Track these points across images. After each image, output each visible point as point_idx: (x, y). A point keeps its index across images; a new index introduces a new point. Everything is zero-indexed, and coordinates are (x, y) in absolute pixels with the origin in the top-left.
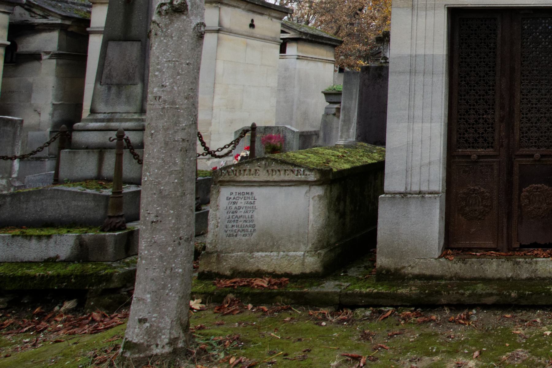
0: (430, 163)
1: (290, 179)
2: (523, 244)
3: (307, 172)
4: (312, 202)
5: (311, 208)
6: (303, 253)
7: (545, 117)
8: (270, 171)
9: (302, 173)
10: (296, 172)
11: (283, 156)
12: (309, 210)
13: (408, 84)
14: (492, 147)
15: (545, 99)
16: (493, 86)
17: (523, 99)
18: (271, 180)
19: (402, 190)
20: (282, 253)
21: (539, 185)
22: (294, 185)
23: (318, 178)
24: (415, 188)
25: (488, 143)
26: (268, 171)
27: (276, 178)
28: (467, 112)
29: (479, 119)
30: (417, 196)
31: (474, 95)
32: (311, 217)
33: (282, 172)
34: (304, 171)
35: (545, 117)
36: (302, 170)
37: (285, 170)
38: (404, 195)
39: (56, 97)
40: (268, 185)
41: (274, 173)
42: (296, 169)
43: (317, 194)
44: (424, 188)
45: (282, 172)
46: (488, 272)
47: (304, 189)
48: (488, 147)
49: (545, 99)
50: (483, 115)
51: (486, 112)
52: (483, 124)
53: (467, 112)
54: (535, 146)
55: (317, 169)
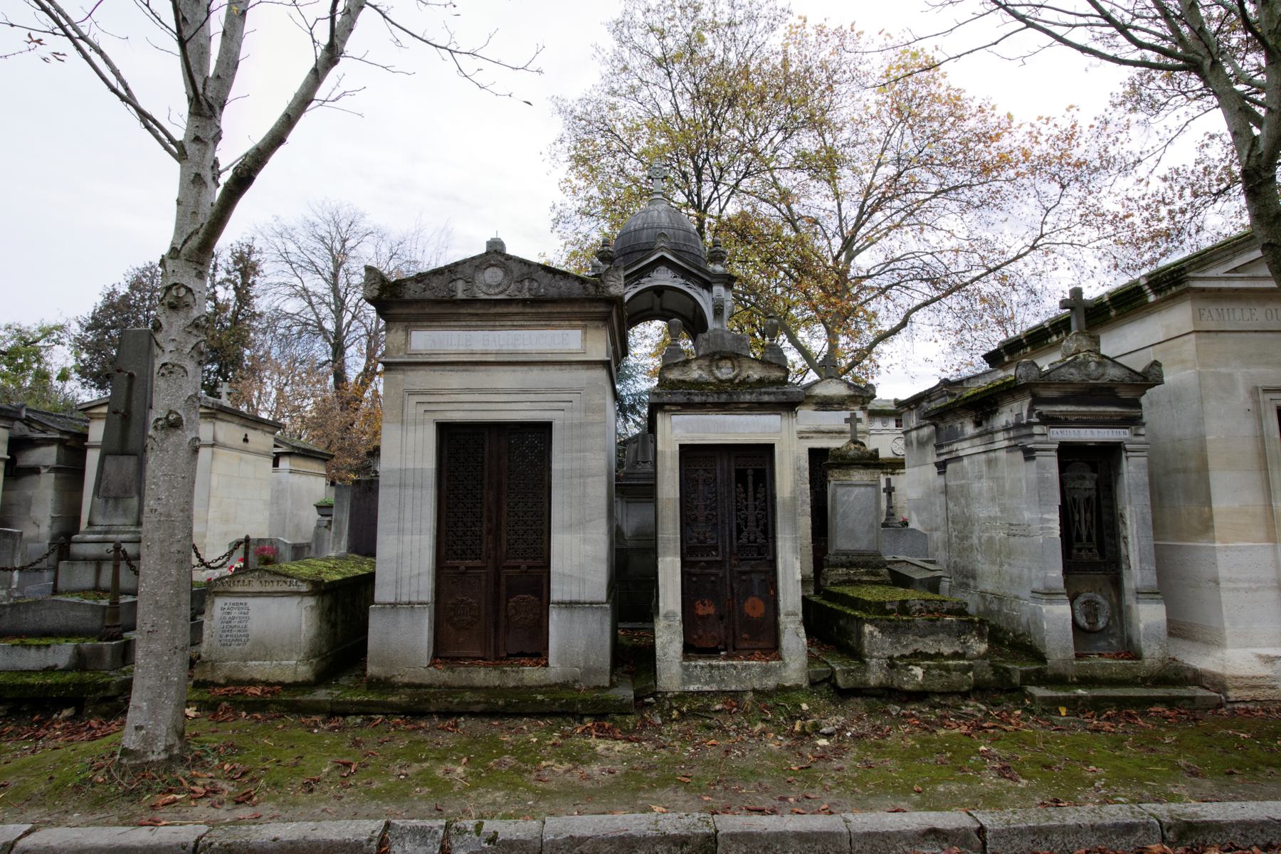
19: (393, 600)
24: (405, 599)
27: (269, 588)
32: (304, 627)
44: (414, 599)
47: (296, 600)
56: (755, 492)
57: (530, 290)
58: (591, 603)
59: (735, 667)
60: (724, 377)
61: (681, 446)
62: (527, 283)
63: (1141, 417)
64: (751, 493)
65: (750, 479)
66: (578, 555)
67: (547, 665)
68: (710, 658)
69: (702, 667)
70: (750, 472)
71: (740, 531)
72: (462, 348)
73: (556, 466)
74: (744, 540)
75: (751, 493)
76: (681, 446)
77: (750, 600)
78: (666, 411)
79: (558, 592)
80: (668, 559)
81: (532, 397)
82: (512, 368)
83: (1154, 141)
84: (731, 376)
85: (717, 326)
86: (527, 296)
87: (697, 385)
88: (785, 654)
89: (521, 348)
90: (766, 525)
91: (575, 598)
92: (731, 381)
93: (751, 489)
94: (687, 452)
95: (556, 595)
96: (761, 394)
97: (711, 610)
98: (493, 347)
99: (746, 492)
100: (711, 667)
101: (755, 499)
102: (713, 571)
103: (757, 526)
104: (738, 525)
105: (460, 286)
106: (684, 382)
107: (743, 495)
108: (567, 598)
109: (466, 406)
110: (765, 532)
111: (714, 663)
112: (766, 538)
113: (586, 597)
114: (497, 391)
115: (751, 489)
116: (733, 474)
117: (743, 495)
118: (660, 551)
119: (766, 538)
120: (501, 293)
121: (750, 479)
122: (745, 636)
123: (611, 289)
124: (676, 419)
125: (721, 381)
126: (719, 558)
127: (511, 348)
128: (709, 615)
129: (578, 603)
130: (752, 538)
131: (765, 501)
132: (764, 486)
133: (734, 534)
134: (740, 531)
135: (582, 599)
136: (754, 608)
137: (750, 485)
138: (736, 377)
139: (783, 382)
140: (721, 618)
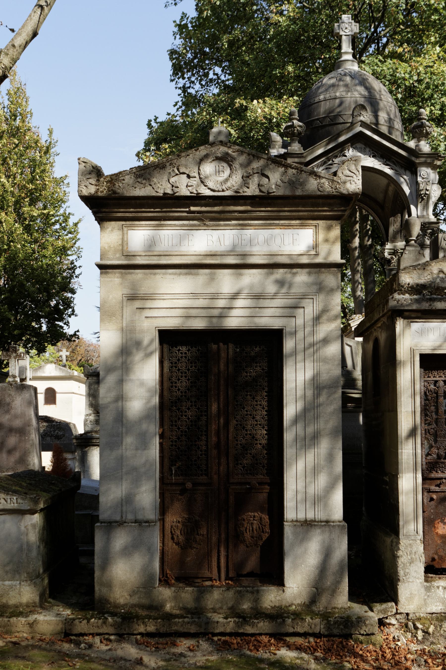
30: (133, 524)
34: (17, 499)
78: (405, 318)
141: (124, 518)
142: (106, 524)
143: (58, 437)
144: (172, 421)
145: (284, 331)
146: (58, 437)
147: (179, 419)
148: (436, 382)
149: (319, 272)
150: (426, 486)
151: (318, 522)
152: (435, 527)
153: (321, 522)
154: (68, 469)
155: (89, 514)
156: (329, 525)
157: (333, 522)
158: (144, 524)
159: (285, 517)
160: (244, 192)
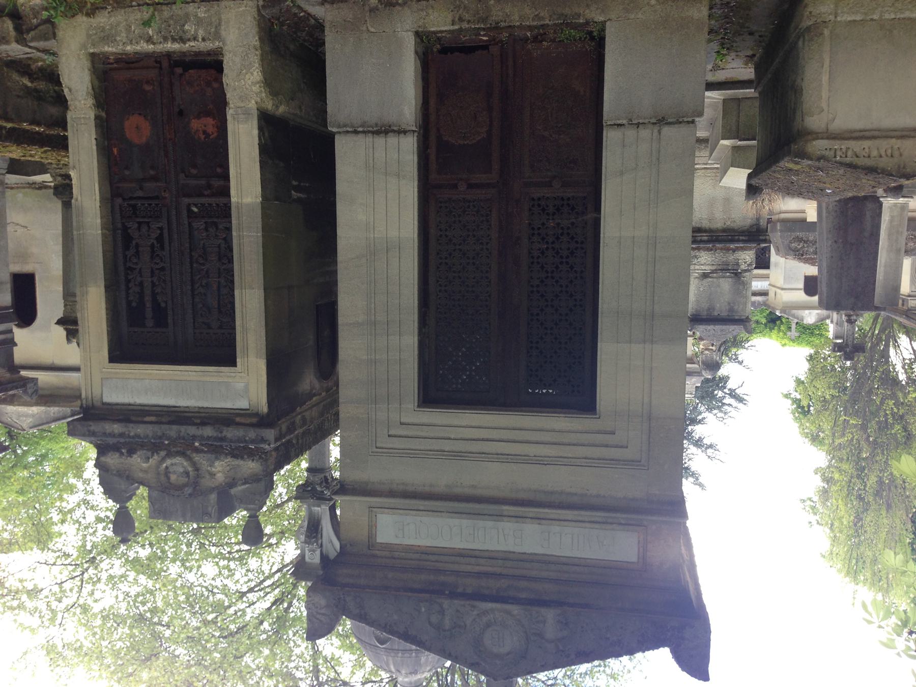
0: (622, 173)
1: (860, 142)
2: (485, 52)
3: (830, 154)
4: (824, 105)
5: (825, 94)
6: (839, 19)
7: (455, 244)
8: (896, 153)
9: (839, 153)
10: (850, 153)
11: (65, 421)
12: (830, 91)
13: (656, 298)
14: (533, 199)
15: (454, 272)
16: (532, 292)
17: (487, 272)
18: (894, 140)
19: (666, 130)
20: (875, 17)
21: (461, 142)
22: (855, 131)
23: (809, 145)
24: (645, 133)
25: (539, 205)
26: (901, 155)
27: (884, 145)
28: (572, 253)
29: (553, 243)
30: (641, 121)
31: (560, 278)
32: (825, 78)
33: (875, 153)
34: (835, 157)
35: (455, 244)
36: (838, 158)
37: (869, 157)
38: (661, 122)
39: (96, 134)
40: (903, 130)
41: (889, 152)
42: (848, 160)
43: (815, 117)
44: (631, 133)
45: (875, 153)
46: (813, 271)
47: (839, 124)
48: (539, 199)
49: (454, 272)
50: (547, 249)
51: (543, 253)
52: (547, 235)
53: (572, 253)
54: (469, 202)
55: (809, 158)
56: (141, 295)
57: (442, 612)
58: (356, 132)
59: (149, 40)
60: (178, 460)
61: (233, 363)
62: (447, 623)
63: (13, 339)
64: (148, 292)
65: (149, 313)
66: (379, 205)
67: (417, 34)
68: (183, 54)
69: (195, 39)
70: (150, 323)
71: (160, 239)
72: (556, 528)
73: (411, 341)
74: (155, 225)
75: (148, 292)
76: (233, 363)
77: (144, 140)
78: (256, 414)
79: (407, 148)
80: (248, 200)
81: (447, 446)
82: (479, 492)
83: (235, 589)
84: (169, 462)
85: (316, 509)
86: (446, 603)
87: (216, 449)
88: (87, 64)
89: (465, 522)
90: (127, 247)
91: (380, 141)
92: (169, 455)
93: (148, 298)
94: (223, 354)
95: (409, 145)
96: (121, 435)
97: (196, 125)
98: (508, 526)
99: (154, 295)
100: (183, 40)
101: (141, 284)
102: (193, 182)
103: (137, 246)
104: (162, 248)
105: (551, 631)
106: (235, 456)
107: (158, 290)
108: (392, 140)
109: (547, 437)
110: (127, 239)
111: (176, 46)
112: (125, 229)
113: (363, 141)
114: (501, 457)
115: (148, 298)
116: (170, 321)
117: (158, 290)
118: (259, 211)
119: (125, 229)
120: (485, 612)
121: (149, 313)
122: (147, 88)
123: (323, 602)
124: (242, 404)
125: (183, 454)
126: (186, 200)
127: (481, 523)
128: (198, 117)
129: (377, 133)
130: (144, 229)
131: (128, 281)
132: (129, 303)
133: (166, 235)
134: (160, 239)
135: (369, 139)
136: (138, 129)
137: (148, 305)
138: (163, 460)
139: (102, 450)
140: (181, 113)
141: (656, 131)
142: (685, 120)
143: (800, 240)
144: (582, 278)
145: (416, 404)
146: (800, 240)
147: (571, 282)
148: (220, 327)
149: (711, 309)
150: (67, 181)
151: (369, 132)
152: (217, 127)
153: (364, 132)
154: (104, 231)
155: (740, 140)
156: (352, 126)
157: (348, 132)
158: (624, 122)
159: (415, 138)
160: (464, 606)
